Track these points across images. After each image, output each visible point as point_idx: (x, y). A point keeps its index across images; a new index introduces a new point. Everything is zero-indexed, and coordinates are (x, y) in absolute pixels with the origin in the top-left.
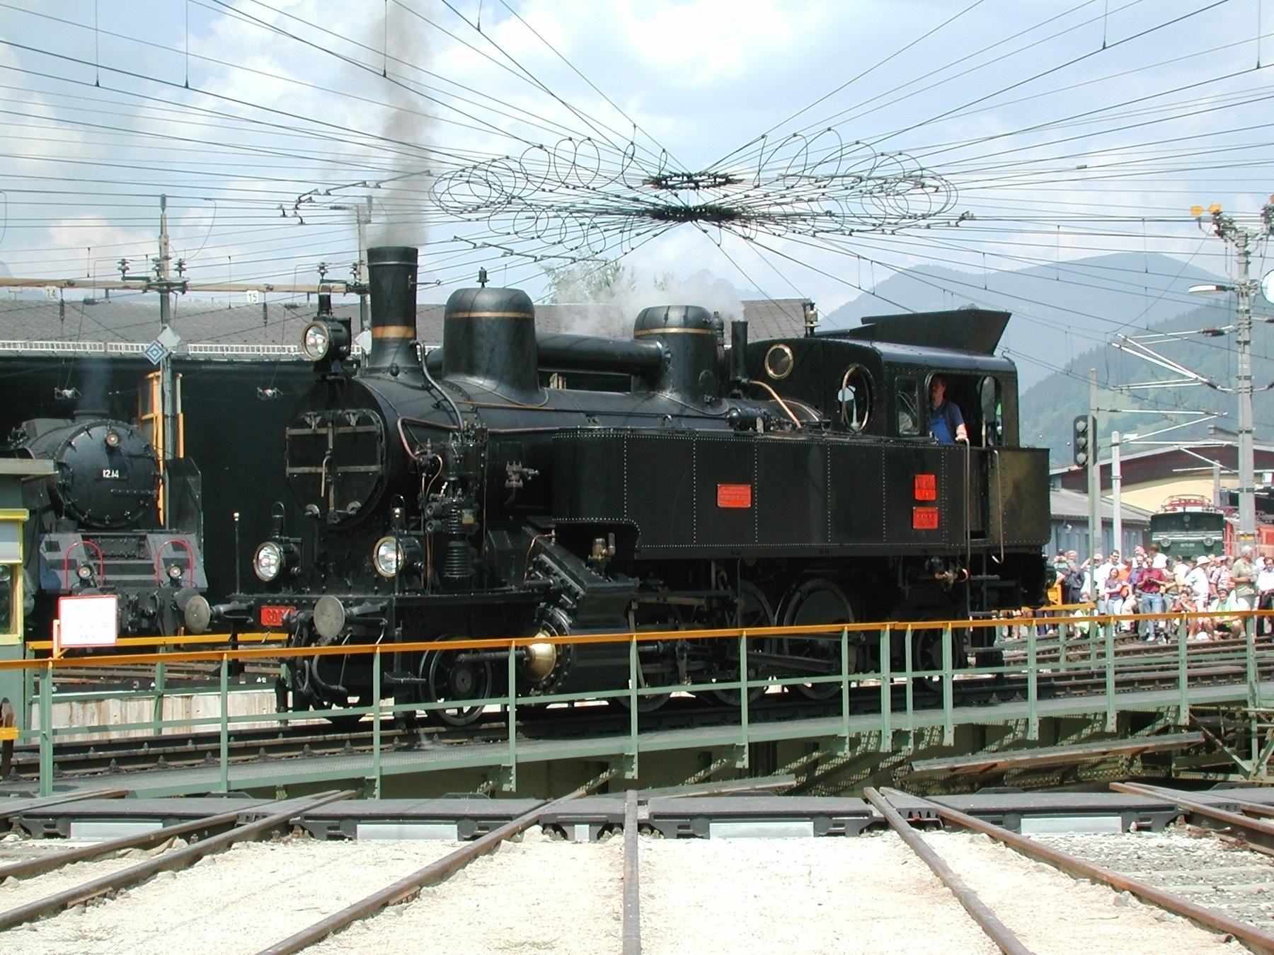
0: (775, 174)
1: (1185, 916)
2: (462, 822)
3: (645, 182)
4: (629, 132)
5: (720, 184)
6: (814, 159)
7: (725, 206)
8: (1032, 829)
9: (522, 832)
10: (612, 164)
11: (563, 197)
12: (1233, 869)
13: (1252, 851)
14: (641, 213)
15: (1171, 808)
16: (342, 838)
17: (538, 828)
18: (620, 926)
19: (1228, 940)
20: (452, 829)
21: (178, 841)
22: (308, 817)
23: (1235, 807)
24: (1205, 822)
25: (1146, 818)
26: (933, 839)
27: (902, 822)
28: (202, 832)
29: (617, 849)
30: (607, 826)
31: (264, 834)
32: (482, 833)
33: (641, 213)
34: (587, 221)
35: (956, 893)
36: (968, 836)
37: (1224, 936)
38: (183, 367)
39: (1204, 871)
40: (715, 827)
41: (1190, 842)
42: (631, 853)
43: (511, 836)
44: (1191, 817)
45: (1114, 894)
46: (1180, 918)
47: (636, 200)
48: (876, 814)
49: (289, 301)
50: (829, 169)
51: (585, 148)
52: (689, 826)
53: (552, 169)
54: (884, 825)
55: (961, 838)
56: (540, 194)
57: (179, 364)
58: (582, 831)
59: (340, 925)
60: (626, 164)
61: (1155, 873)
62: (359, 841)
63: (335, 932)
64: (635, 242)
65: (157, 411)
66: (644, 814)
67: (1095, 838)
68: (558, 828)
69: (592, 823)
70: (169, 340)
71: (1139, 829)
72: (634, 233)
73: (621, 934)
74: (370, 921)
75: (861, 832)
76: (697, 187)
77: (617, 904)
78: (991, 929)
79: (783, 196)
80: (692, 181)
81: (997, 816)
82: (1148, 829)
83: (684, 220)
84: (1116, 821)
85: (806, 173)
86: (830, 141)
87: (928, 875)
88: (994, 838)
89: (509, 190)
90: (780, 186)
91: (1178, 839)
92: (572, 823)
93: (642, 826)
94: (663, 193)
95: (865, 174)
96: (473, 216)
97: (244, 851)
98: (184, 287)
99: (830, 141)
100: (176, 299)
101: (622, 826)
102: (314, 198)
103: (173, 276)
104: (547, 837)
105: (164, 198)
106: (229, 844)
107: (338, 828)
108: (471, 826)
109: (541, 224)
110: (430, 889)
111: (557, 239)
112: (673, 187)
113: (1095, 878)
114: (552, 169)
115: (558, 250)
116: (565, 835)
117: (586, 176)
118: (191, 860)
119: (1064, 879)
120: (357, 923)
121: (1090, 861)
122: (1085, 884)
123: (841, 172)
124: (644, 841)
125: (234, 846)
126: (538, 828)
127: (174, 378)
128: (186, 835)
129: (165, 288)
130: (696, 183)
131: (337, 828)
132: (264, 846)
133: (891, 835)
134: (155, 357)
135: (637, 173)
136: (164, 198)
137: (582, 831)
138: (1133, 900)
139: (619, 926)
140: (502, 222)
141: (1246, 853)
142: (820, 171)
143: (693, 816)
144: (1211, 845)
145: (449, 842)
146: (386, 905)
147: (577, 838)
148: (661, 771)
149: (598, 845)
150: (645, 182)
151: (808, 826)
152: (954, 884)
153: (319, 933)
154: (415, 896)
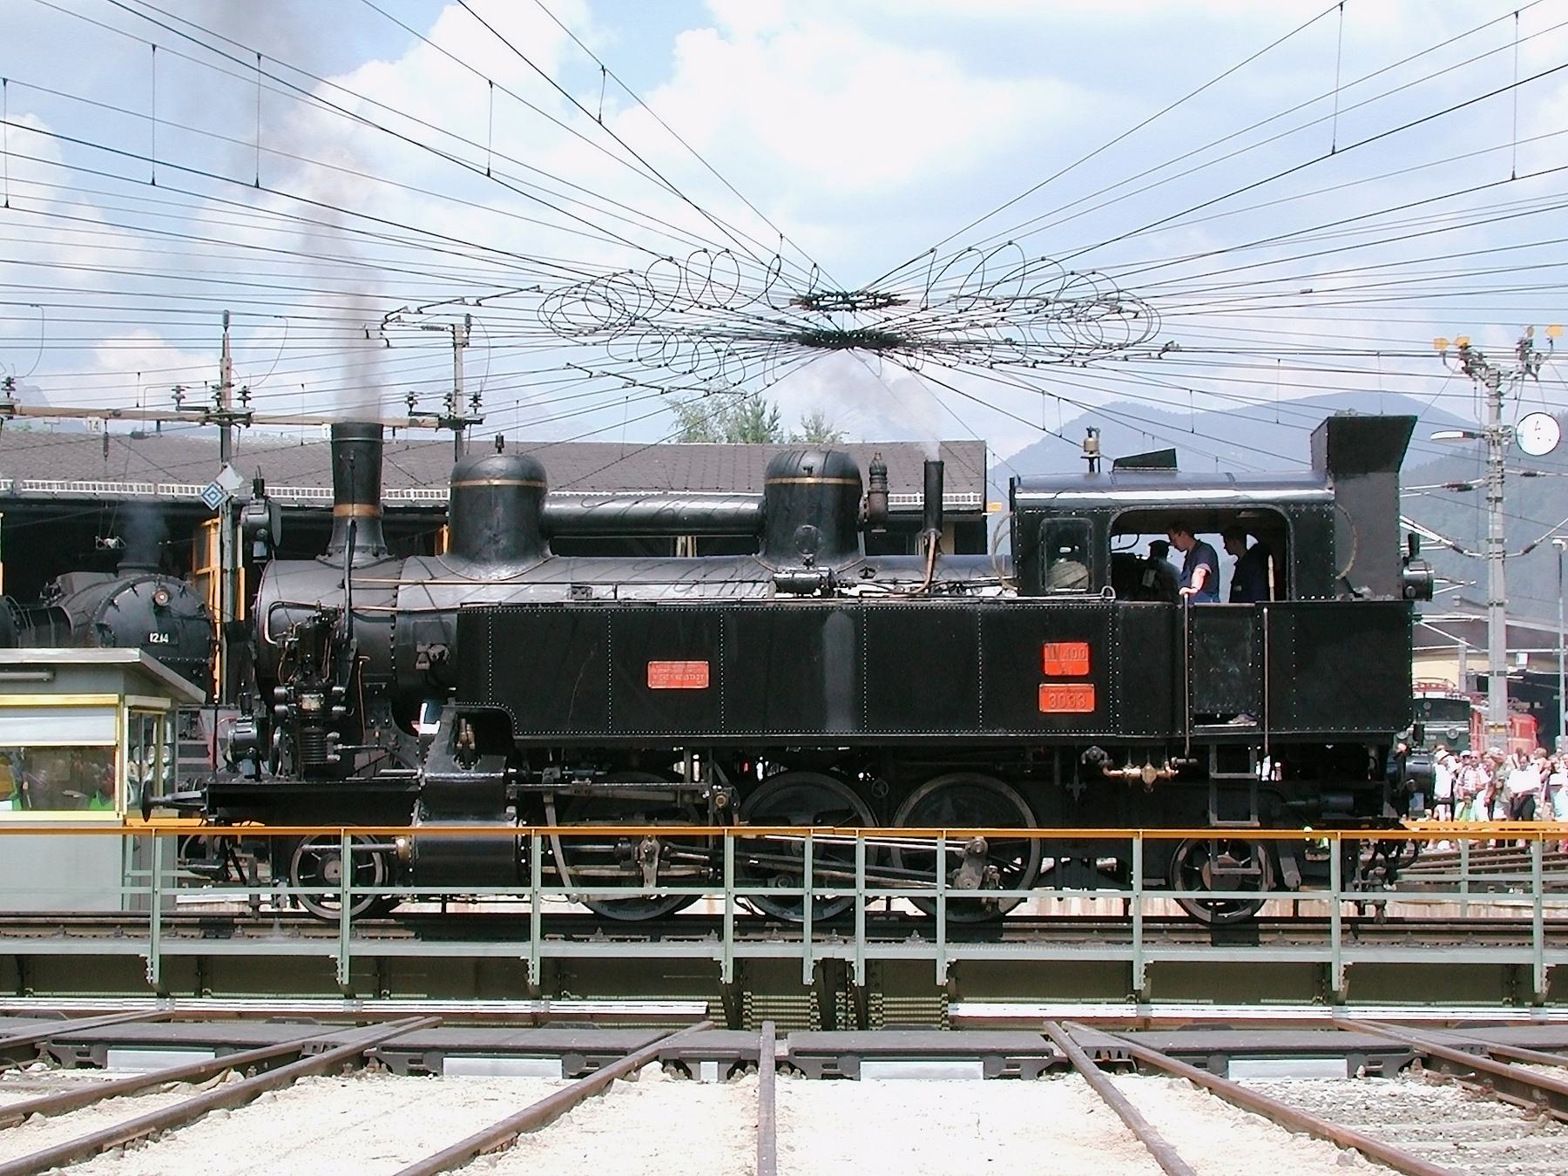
0: (945, 295)
3: (792, 302)
5: (881, 305)
6: (991, 277)
7: (886, 331)
8: (1242, 1073)
9: (638, 1068)
10: (754, 280)
13: (1501, 1101)
14: (788, 339)
15: (1406, 1050)
16: (426, 1073)
17: (657, 1065)
20: (556, 1065)
21: (233, 1073)
22: (384, 1049)
23: (1481, 1049)
26: (1125, 1083)
27: (1088, 1063)
28: (261, 1064)
29: (750, 1091)
30: (739, 1064)
31: (334, 1068)
32: (592, 1068)
33: (788, 339)
34: (723, 346)
36: (1166, 1080)
39: (1443, 1125)
40: (867, 1067)
41: (1428, 1090)
42: (767, 1097)
43: (625, 1074)
48: (1057, 1053)
51: (723, 262)
52: (836, 1066)
53: (683, 285)
54: (1066, 1066)
55: (1158, 1083)
56: (668, 315)
58: (709, 1069)
60: (770, 280)
61: (1385, 1127)
65: (215, 564)
66: (782, 1049)
69: (720, 1060)
71: (1368, 1074)
72: (778, 361)
75: (1040, 1074)
76: (854, 308)
80: (849, 302)
81: (1201, 1057)
82: (1377, 1074)
84: (1340, 1065)
85: (983, 294)
87: (1118, 1125)
88: (1196, 1083)
89: (632, 310)
90: (952, 308)
92: (699, 1060)
93: (779, 1064)
94: (814, 315)
95: (1052, 296)
97: (310, 1087)
98: (248, 419)
99: (1011, 257)
100: (240, 433)
102: (403, 316)
103: (236, 406)
104: (667, 1075)
109: (670, 350)
110: (529, 1135)
111: (688, 367)
112: (825, 308)
113: (1316, 1132)
114: (683, 285)
116: (689, 1074)
117: (724, 295)
119: (1278, 1133)
121: (1310, 1111)
122: (1304, 1139)
124: (783, 1082)
126: (657, 1065)
128: (243, 1067)
130: (853, 304)
133: (1074, 1079)
134: (213, 502)
137: (709, 1069)
138: (1360, 1159)
140: (624, 346)
141: (1493, 1104)
142: (998, 292)
144: (1451, 1094)
145: (552, 1080)
146: (477, 1153)
150: (792, 302)
151: (977, 1066)
154: (512, 1143)
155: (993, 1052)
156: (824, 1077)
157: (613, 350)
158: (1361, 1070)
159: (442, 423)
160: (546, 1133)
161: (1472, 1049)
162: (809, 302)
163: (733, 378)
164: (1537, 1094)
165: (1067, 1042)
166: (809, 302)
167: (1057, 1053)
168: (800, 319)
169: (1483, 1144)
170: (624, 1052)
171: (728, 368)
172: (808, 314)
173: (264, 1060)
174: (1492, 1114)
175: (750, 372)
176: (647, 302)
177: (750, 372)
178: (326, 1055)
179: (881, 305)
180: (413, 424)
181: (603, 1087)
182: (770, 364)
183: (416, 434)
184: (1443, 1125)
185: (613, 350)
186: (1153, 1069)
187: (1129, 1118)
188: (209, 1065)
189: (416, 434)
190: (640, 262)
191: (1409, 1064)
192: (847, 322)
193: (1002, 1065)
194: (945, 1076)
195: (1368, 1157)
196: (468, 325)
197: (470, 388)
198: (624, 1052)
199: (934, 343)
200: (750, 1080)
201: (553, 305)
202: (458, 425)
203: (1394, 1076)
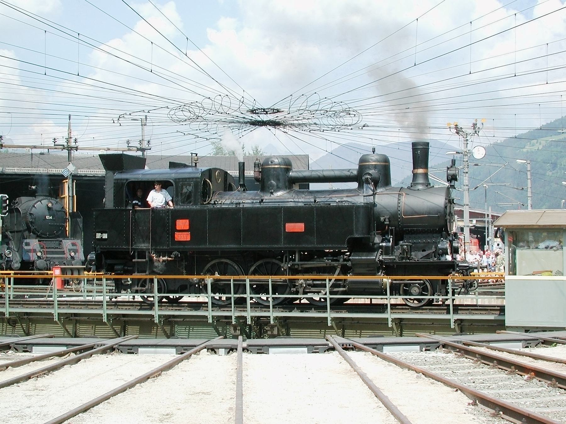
0: (295, 109)
1: (441, 382)
3: (247, 111)
8: (388, 351)
9: (200, 351)
11: (218, 117)
12: (459, 365)
15: (437, 343)
16: (133, 353)
17: (206, 350)
18: (235, 386)
19: (457, 391)
20: (174, 350)
22: (120, 346)
23: (461, 342)
24: (449, 348)
26: (350, 353)
28: (81, 351)
29: (235, 358)
30: (231, 349)
31: (104, 352)
34: (226, 125)
35: (358, 374)
36: (364, 353)
37: (455, 389)
38: (76, 178)
40: (271, 350)
42: (240, 360)
43: (195, 353)
50: (315, 107)
51: (226, 99)
52: (261, 350)
54: (333, 349)
55: (361, 354)
56: (208, 115)
57: (75, 177)
58: (222, 351)
61: (431, 366)
62: (139, 354)
64: (244, 133)
66: (245, 345)
67: (410, 354)
68: (213, 350)
70: (71, 168)
71: (426, 350)
72: (243, 130)
73: (235, 389)
75: (325, 351)
76: (267, 113)
77: (234, 378)
80: (265, 112)
81: (375, 346)
82: (429, 350)
87: (349, 367)
88: (373, 354)
90: (297, 113)
91: (440, 354)
94: (254, 116)
95: (328, 110)
96: (184, 123)
97: (97, 358)
98: (77, 149)
100: (74, 153)
102: (125, 116)
103: (73, 144)
104: (209, 353)
108: (182, 349)
109: (209, 127)
110: (165, 372)
112: (258, 113)
113: (410, 368)
116: (215, 352)
117: (226, 109)
118: (78, 360)
120: (138, 385)
124: (245, 355)
126: (206, 350)
127: (73, 182)
128: (75, 352)
129: (70, 149)
132: (104, 356)
135: (244, 108)
137: (222, 351)
138: (423, 376)
140: (195, 125)
141: (464, 359)
143: (263, 346)
144: (452, 356)
145: (173, 355)
146: (149, 378)
149: (228, 356)
150: (247, 111)
151: (305, 349)
155: (310, 345)
156: (258, 353)
158: (424, 349)
161: (458, 342)
162: (253, 111)
164: (477, 356)
165: (333, 341)
166: (253, 111)
169: (461, 371)
170: (195, 346)
173: (82, 350)
176: (202, 111)
190: (199, 99)
191: (438, 347)
195: (426, 376)
198: (195, 346)
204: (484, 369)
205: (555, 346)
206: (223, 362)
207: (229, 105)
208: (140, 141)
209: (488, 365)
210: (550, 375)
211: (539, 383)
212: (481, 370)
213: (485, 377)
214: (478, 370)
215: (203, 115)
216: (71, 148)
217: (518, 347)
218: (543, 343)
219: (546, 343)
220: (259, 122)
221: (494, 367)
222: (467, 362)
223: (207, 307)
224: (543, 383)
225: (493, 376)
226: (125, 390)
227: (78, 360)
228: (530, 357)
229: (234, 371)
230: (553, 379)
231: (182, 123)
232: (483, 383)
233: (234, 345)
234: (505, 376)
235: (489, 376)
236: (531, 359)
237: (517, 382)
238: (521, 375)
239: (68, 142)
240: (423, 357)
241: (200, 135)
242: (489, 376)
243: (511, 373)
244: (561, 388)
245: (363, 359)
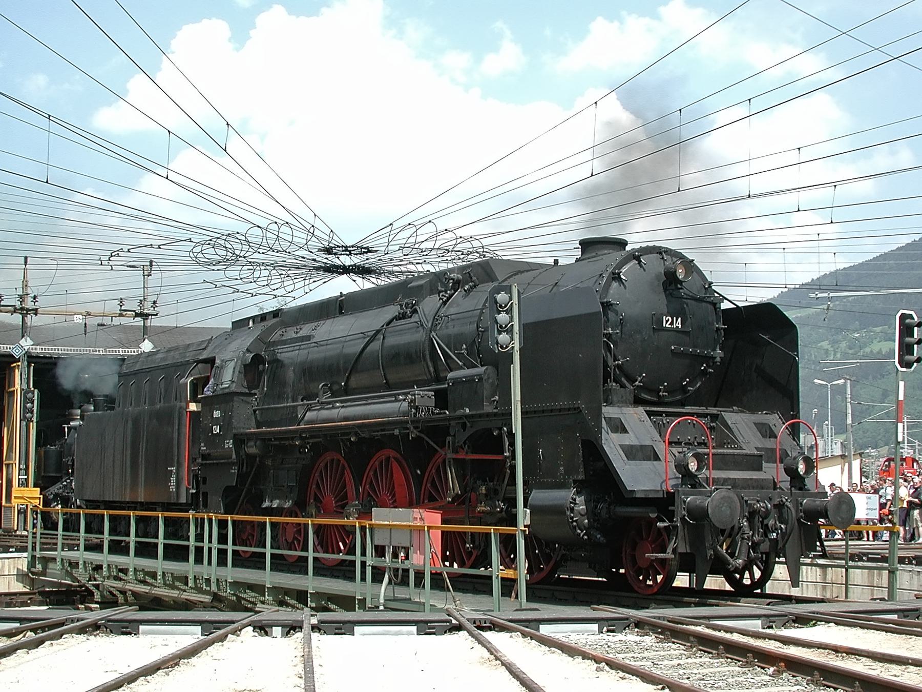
0: (397, 248)
1: (637, 676)
2: (204, 625)
3: (319, 250)
4: (311, 219)
5: (365, 252)
6: (419, 239)
7: (367, 266)
8: (545, 630)
9: (240, 631)
10: (300, 238)
11: (271, 257)
12: (662, 653)
13: (674, 643)
14: (317, 269)
15: (627, 619)
16: (130, 634)
17: (250, 628)
18: (302, 681)
19: (663, 688)
20: (198, 629)
21: (29, 633)
22: (109, 621)
23: (664, 618)
24: (646, 627)
25: (611, 625)
26: (489, 635)
27: (471, 627)
28: (43, 629)
29: (299, 640)
30: (291, 628)
31: (82, 631)
32: (215, 632)
33: (317, 269)
34: (284, 273)
35: (503, 664)
36: (508, 635)
37: (660, 687)
38: (34, 360)
39: (646, 654)
40: (357, 629)
41: (638, 638)
42: (308, 642)
43: (234, 632)
44: (639, 624)
45: (596, 665)
46: (634, 678)
47: (314, 260)
48: (454, 622)
49: (100, 322)
50: (429, 245)
51: (285, 229)
52: (343, 628)
53: (265, 241)
54: (459, 628)
55: (504, 635)
56: (256, 255)
57: (31, 358)
58: (277, 631)
59: (131, 679)
60: (309, 237)
61: (618, 655)
62: (140, 635)
63: (128, 684)
64: (312, 286)
65: (18, 386)
66: (314, 621)
67: (584, 635)
68: (263, 629)
69: (283, 626)
70: (26, 343)
71: (608, 631)
72: (312, 281)
73: (303, 686)
74: (149, 678)
75: (445, 632)
76: (351, 254)
77: (300, 669)
78: (523, 681)
79: (402, 261)
80: (347, 250)
81: (527, 622)
82: (613, 631)
83: (342, 274)
84: (595, 627)
85: (416, 246)
86: (430, 228)
87: (486, 654)
88: (524, 635)
89: (237, 252)
90: (400, 253)
91: (630, 636)
92: (271, 626)
93: (314, 628)
94: (330, 257)
95: (451, 248)
96: (215, 268)
97: (70, 639)
98: (36, 311)
99: (430, 228)
100: (31, 320)
101: (301, 628)
102: (120, 254)
103: (29, 304)
104: (256, 634)
105: (26, 258)
106: (60, 636)
107: (127, 628)
108: (208, 626)
109: (257, 274)
110: (186, 661)
111: (266, 283)
112: (335, 254)
113: (585, 656)
114: (265, 241)
115: (267, 290)
116: (266, 634)
117: (285, 245)
118: (39, 643)
119: (565, 658)
120: (142, 678)
121: (580, 646)
122: (579, 659)
123: (436, 247)
124: (315, 636)
125: (64, 636)
126: (250, 628)
127: (29, 366)
128: (34, 630)
129: (24, 312)
130: (350, 251)
131: (127, 628)
132: (82, 637)
133: (463, 634)
134: (17, 353)
135: (314, 244)
136: (26, 258)
137: (277, 631)
138: (607, 668)
139: (302, 682)
140: (234, 272)
141: (670, 644)
142: (423, 246)
143: (344, 622)
144: (649, 640)
145: (196, 636)
146: (159, 669)
147: (274, 635)
148: (325, 602)
149: (287, 639)
150: (319, 250)
151: (414, 629)
152: (502, 659)
153: (118, 682)
154: (177, 664)
155: (422, 621)
156: (336, 634)
157: (229, 274)
158: (605, 629)
159: (137, 315)
160: (194, 660)
161: (659, 618)
162: (328, 251)
163: (289, 289)
164: (692, 639)
165: (459, 616)
166: (328, 251)
167: (454, 622)
168: (323, 258)
169: (666, 662)
170: (233, 622)
171: (286, 284)
172: (327, 256)
173: (45, 627)
174: (670, 648)
175: (297, 286)
176: (246, 248)
177: (297, 286)
178: (78, 624)
179: (365, 252)
180: (121, 315)
181: (222, 639)
182: (307, 282)
183: (124, 321)
184: (646, 654)
185: (229, 274)
186: (502, 628)
187: (491, 650)
188: (17, 628)
189: (124, 321)
190: (242, 227)
191: (628, 626)
192: (347, 260)
193: (425, 628)
194: (397, 634)
195: (611, 668)
196: (151, 265)
197: (151, 299)
198: (233, 622)
199: (390, 272)
200: (299, 635)
201: (198, 249)
202: (145, 316)
203: (621, 632)
204: (703, 660)
205: (814, 625)
206: (281, 649)
207: (290, 238)
208: (21, 297)
209: (709, 653)
210: (810, 666)
211: (793, 680)
212: (698, 660)
213: (706, 671)
214: (694, 660)
215: (248, 254)
216: (28, 310)
217: (756, 625)
218: (794, 621)
219: (802, 621)
220: (338, 267)
221: (719, 656)
222: (675, 649)
223: (56, 544)
224: (799, 679)
225: (719, 669)
226: (121, 686)
227: (41, 642)
228: (776, 640)
229: (299, 659)
230: (816, 673)
231: (214, 268)
232: (703, 680)
233: (298, 621)
234: (738, 669)
235: (711, 670)
236: (778, 644)
237: (757, 678)
238: (763, 668)
239: (22, 298)
240: (604, 642)
241: (241, 288)
242: (711, 670)
243: (748, 664)
244: (829, 687)
245: (509, 644)
